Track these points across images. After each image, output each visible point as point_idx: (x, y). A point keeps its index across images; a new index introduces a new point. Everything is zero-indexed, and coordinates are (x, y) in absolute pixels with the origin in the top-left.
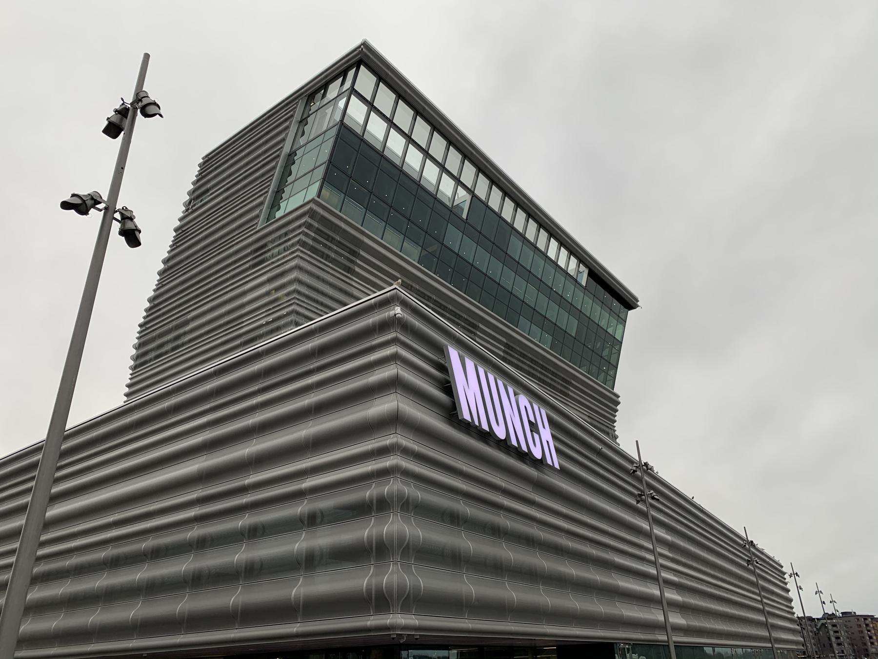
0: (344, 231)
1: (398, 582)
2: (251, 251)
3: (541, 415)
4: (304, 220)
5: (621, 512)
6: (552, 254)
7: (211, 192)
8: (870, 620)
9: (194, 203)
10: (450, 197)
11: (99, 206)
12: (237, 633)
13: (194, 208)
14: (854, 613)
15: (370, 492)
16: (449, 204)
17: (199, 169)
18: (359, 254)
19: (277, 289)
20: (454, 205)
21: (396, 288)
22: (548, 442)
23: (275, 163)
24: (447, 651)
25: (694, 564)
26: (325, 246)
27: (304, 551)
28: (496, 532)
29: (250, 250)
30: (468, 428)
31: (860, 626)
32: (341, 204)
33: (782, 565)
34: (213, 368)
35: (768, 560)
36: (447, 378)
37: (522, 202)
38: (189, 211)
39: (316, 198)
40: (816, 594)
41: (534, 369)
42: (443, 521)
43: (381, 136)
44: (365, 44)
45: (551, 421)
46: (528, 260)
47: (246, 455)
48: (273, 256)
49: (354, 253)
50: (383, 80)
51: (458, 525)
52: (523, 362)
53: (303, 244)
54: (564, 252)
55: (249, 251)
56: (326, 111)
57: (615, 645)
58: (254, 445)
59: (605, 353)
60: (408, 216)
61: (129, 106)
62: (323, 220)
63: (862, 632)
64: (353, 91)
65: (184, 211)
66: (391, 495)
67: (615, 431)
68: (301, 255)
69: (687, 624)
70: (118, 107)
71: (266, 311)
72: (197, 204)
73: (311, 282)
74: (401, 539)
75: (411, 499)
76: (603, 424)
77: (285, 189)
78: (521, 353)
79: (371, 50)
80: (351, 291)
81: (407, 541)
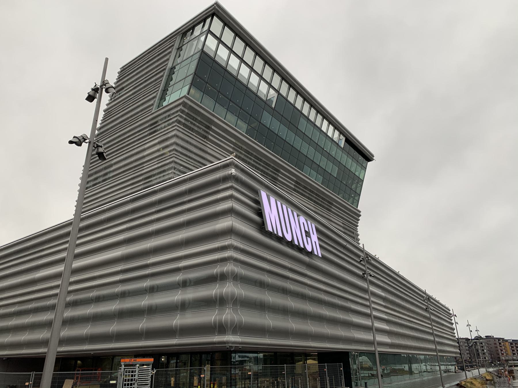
0: (203, 114)
1: (230, 319)
2: (149, 125)
3: (312, 227)
4: (180, 108)
5: (356, 280)
6: (324, 129)
7: (125, 89)
8: (502, 340)
9: (115, 95)
10: (265, 93)
11: (86, 141)
12: (143, 343)
13: (115, 98)
14: (493, 336)
15: (216, 270)
16: (264, 99)
17: (118, 75)
18: (211, 128)
19: (164, 148)
20: (268, 99)
21: (232, 158)
22: (315, 242)
23: (163, 73)
24: (257, 354)
25: (397, 309)
26: (192, 123)
27: (180, 303)
28: (284, 291)
29: (148, 129)
30: (271, 235)
31: (495, 344)
32: (201, 98)
33: (450, 309)
34: (130, 198)
35: (441, 307)
36: (260, 207)
37: (308, 98)
38: (113, 100)
39: (187, 95)
40: (467, 326)
41: (312, 195)
42: (256, 286)
43: (225, 58)
44: (217, 4)
45: (317, 230)
46: (309, 132)
47: (148, 247)
48: (161, 129)
49: (209, 128)
50: (227, 25)
51: (264, 288)
52: (305, 192)
53: (179, 122)
54: (331, 128)
55: (147, 125)
56: (194, 43)
57: (350, 353)
58: (152, 242)
59: (354, 187)
60: (240, 106)
61: (99, 87)
62: (191, 108)
63: (497, 347)
64: (209, 31)
65: (109, 100)
66: (228, 272)
67: (357, 231)
68: (178, 128)
69: (391, 342)
70: (93, 87)
71: (157, 161)
72: (117, 96)
73: (183, 144)
74: (233, 273)
75: (238, 274)
76: (350, 227)
77: (168, 89)
78: (304, 186)
79: (220, 7)
80: (206, 150)
81: (236, 297)
